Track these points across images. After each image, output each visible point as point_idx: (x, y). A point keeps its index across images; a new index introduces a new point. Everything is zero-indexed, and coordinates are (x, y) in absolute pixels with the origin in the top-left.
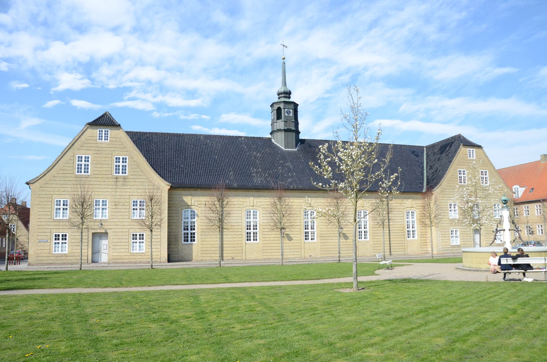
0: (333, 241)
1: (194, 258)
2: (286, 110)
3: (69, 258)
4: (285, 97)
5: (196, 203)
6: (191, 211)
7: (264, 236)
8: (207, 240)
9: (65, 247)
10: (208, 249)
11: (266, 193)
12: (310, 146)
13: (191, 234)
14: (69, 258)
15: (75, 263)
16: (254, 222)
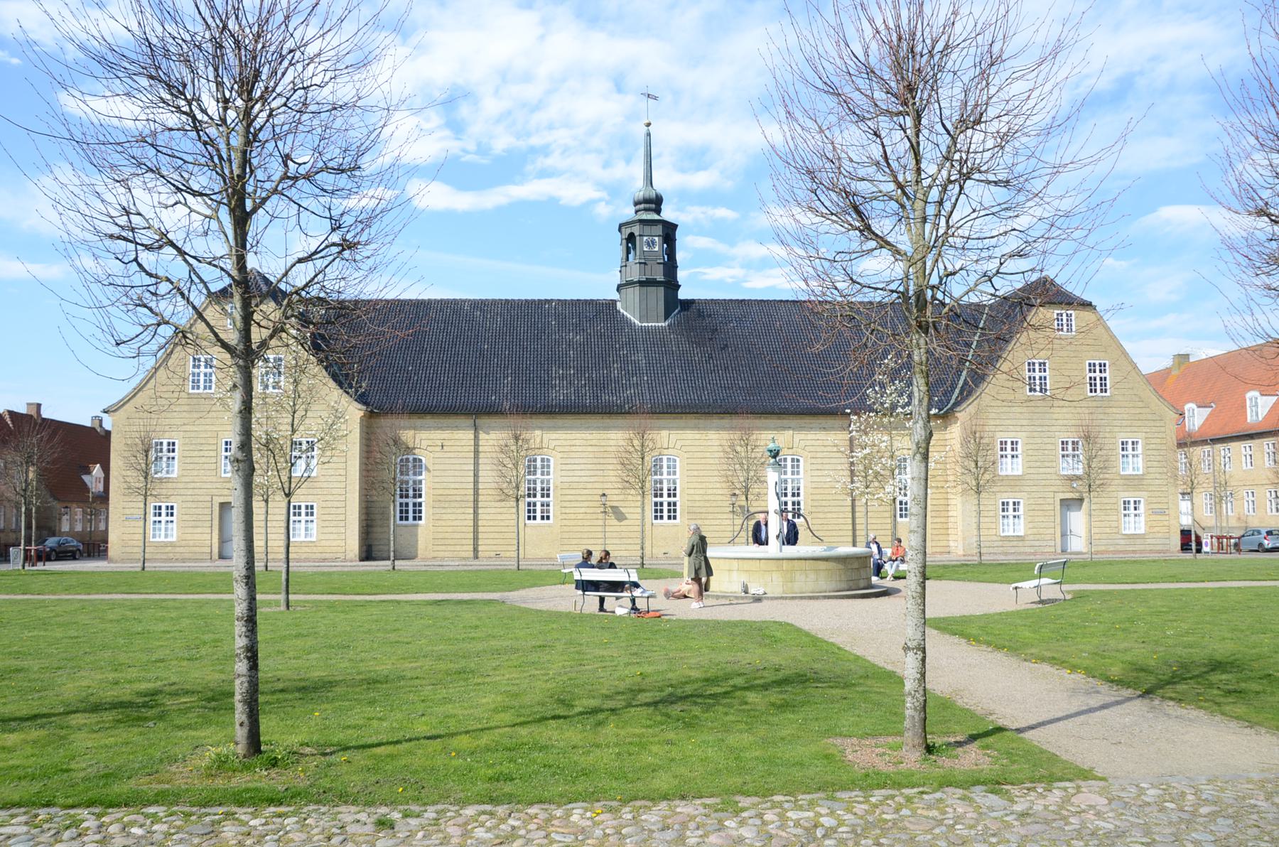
0: (717, 522)
1: (421, 552)
2: (645, 238)
3: (178, 550)
4: (646, 210)
5: (424, 444)
6: (415, 460)
7: (564, 510)
8: (445, 517)
9: (172, 529)
10: (447, 535)
11: (620, 421)
12: (700, 314)
13: (415, 505)
14: (178, 550)
15: (131, 560)
16: (669, 481)
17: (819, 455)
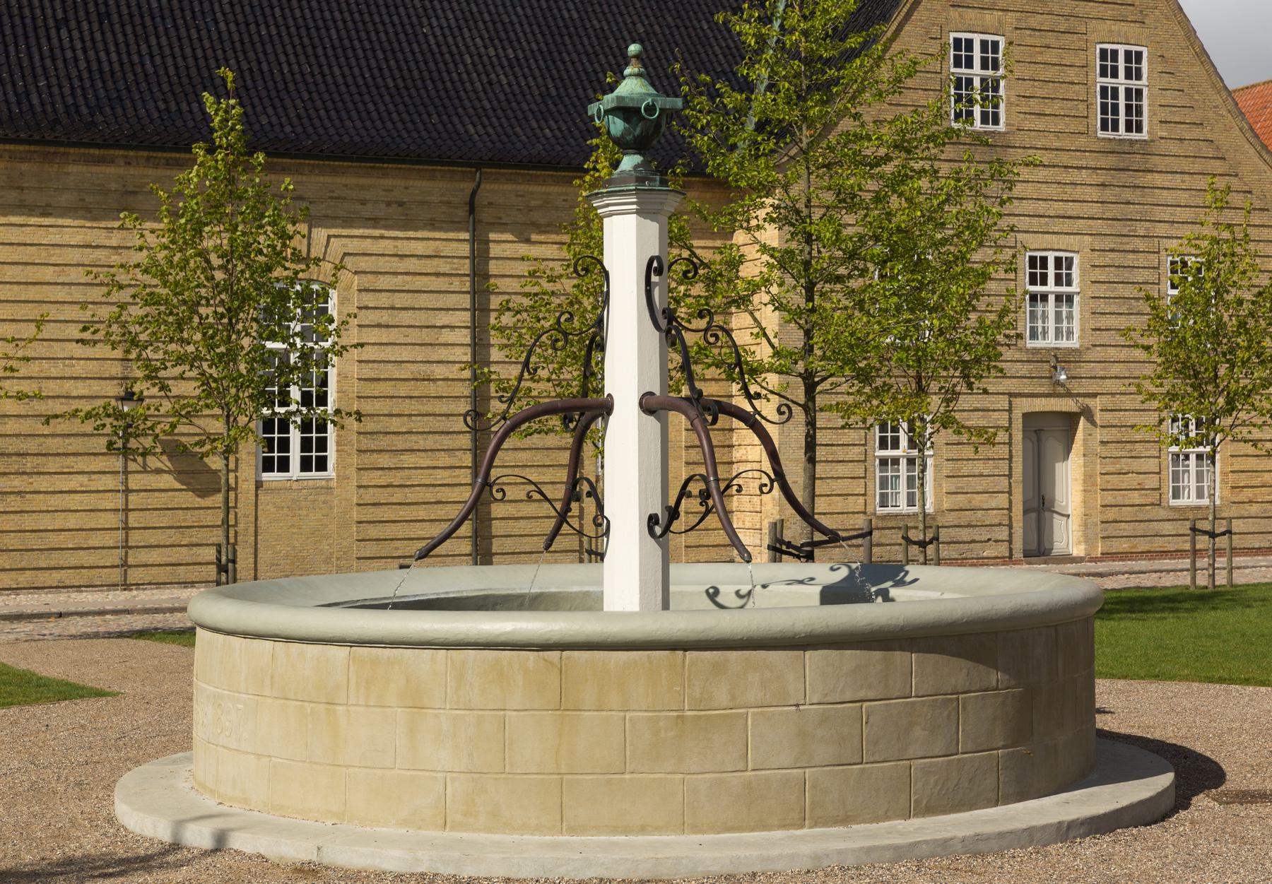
0: (74, 483)
17: (384, 282)
